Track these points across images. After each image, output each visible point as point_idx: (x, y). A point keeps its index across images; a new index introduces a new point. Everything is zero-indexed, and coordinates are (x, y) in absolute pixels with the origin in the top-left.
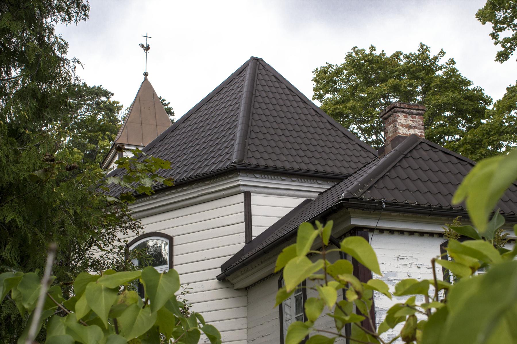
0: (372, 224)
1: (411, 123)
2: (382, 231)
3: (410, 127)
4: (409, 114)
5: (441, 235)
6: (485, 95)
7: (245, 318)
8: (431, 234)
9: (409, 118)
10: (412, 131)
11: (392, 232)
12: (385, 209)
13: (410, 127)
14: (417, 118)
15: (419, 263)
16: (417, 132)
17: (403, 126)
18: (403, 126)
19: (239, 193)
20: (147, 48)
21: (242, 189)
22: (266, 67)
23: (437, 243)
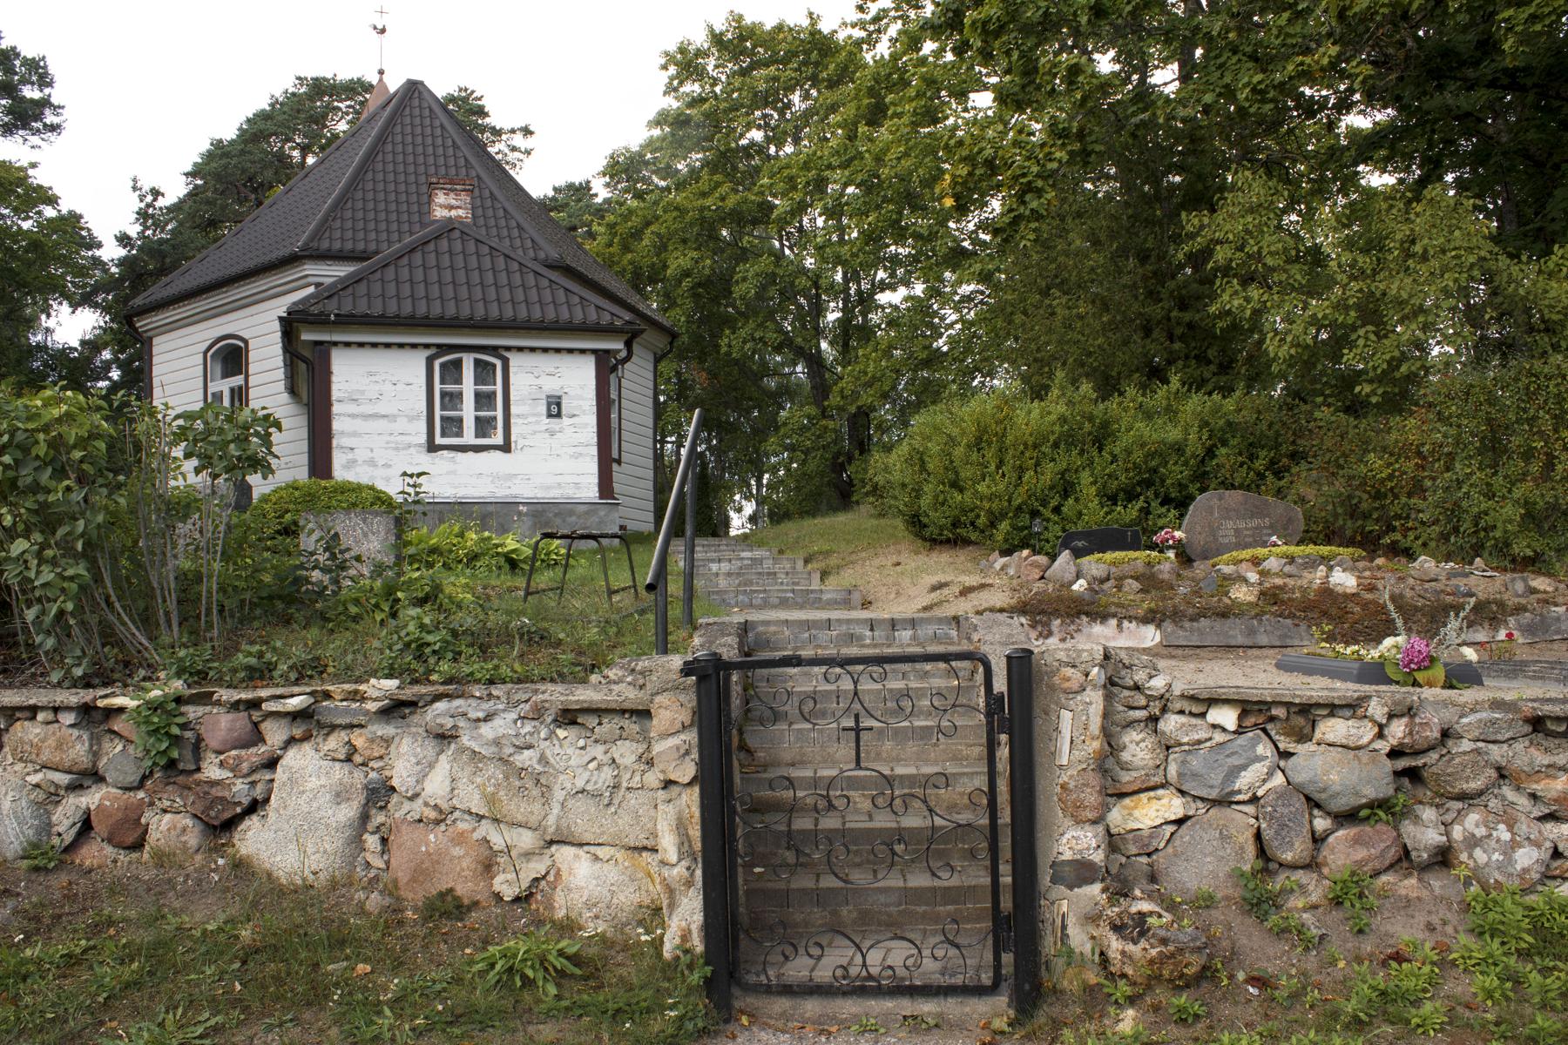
0: (336, 338)
1: (453, 202)
2: (348, 344)
3: (451, 208)
4: (452, 190)
5: (427, 346)
6: (75, 344)
7: (632, 547)
8: (414, 346)
9: (452, 195)
10: (454, 213)
11: (361, 345)
12: (334, 323)
13: (451, 208)
14: (463, 196)
15: (394, 379)
16: (461, 212)
17: (441, 206)
18: (441, 206)
19: (309, 285)
20: (383, 31)
21: (311, 280)
22: (425, 94)
23: (423, 355)
